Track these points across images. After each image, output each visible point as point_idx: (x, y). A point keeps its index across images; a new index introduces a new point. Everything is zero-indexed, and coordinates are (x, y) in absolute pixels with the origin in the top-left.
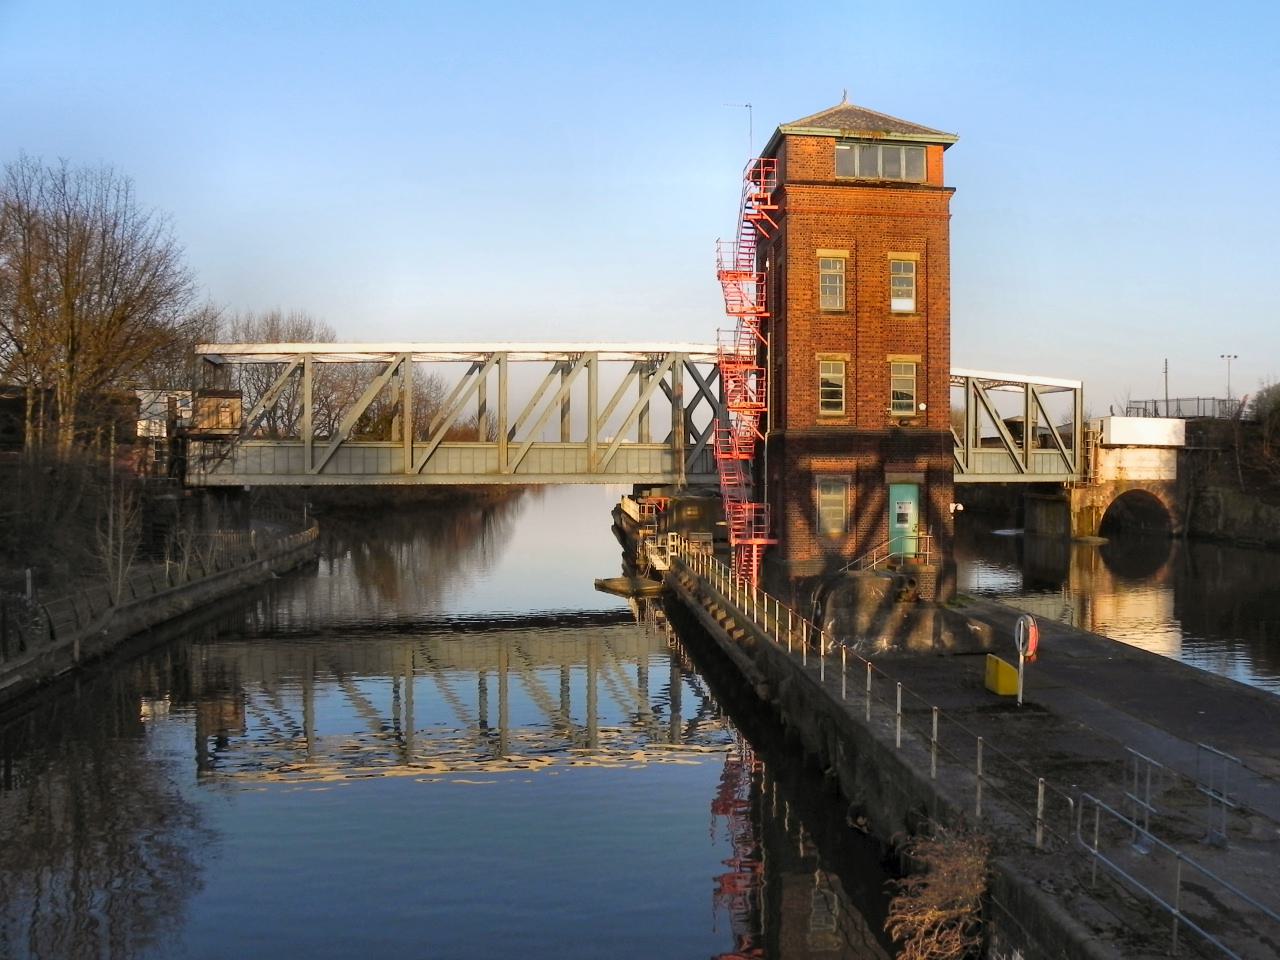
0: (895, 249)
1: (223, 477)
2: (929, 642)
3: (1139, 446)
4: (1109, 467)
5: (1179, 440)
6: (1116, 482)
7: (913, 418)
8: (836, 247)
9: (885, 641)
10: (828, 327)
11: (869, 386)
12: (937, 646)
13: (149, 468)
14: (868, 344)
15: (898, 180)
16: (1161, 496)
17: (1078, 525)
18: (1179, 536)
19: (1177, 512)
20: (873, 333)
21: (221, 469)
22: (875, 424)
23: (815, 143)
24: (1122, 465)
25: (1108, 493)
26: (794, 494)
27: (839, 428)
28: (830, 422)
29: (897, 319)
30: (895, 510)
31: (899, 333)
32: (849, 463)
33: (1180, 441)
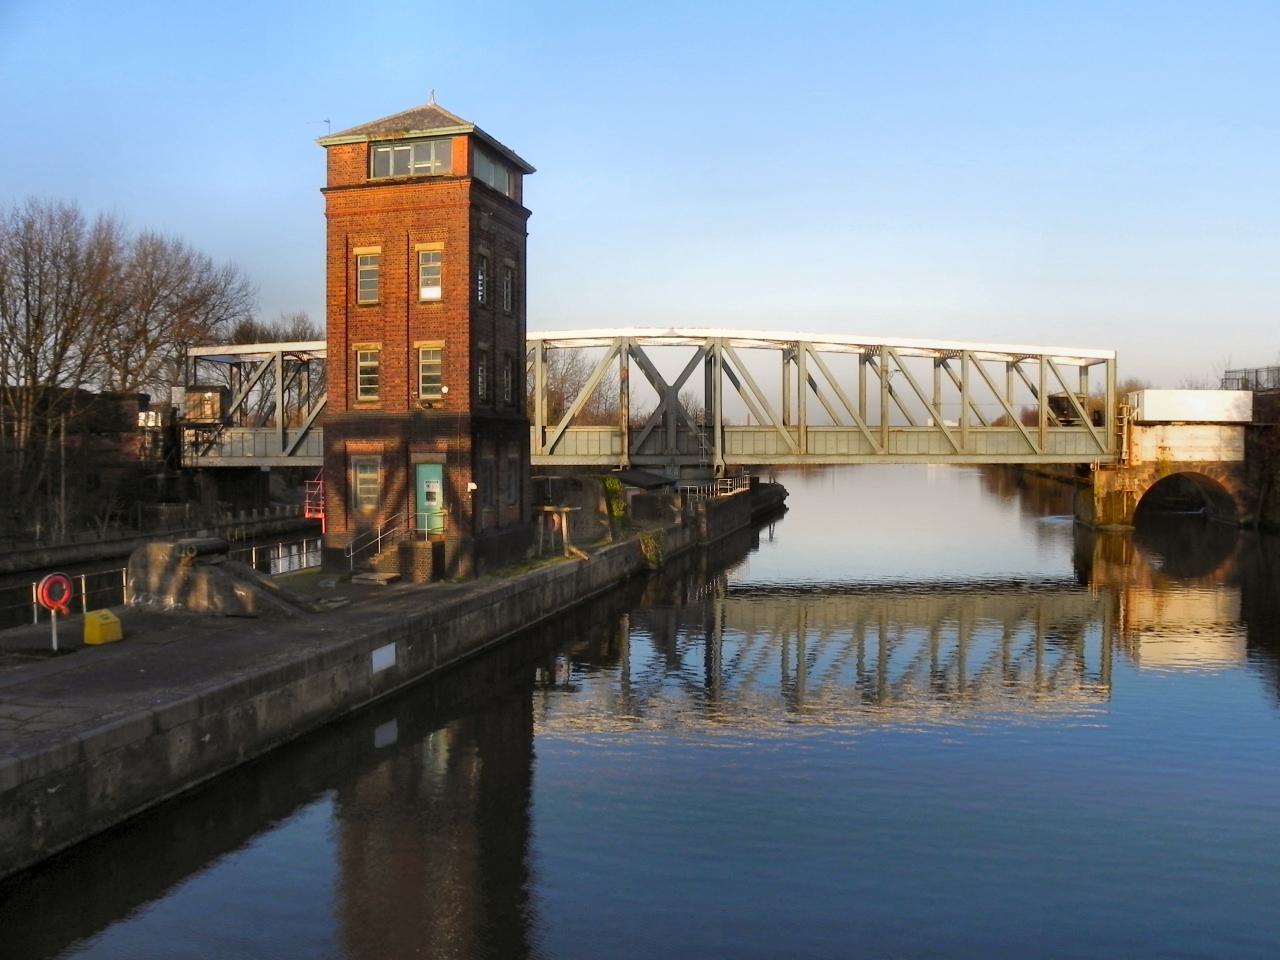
0: (421, 241)
1: (213, 459)
2: (205, 603)
3: (1188, 423)
4: (1145, 448)
5: (1247, 416)
6: (1156, 463)
7: (436, 401)
8: (370, 244)
9: (172, 599)
10: (363, 319)
11: (396, 372)
12: (211, 607)
13: (147, 452)
14: (394, 333)
15: (428, 174)
16: (1221, 480)
17: (1104, 511)
18: (1248, 526)
19: (1245, 499)
20: (399, 322)
21: (211, 453)
22: (401, 407)
23: (350, 150)
24: (1165, 444)
25: (1146, 476)
26: (331, 473)
27: (370, 412)
28: (364, 407)
29: (422, 307)
30: (423, 489)
31: (424, 321)
32: (378, 445)
33: (1247, 416)
